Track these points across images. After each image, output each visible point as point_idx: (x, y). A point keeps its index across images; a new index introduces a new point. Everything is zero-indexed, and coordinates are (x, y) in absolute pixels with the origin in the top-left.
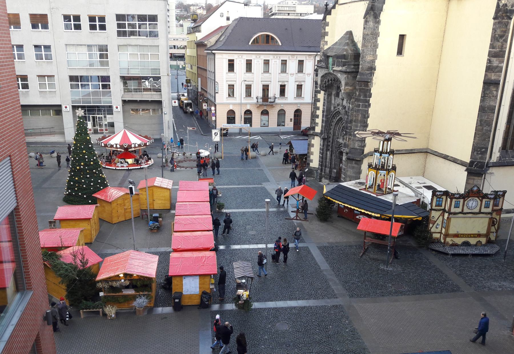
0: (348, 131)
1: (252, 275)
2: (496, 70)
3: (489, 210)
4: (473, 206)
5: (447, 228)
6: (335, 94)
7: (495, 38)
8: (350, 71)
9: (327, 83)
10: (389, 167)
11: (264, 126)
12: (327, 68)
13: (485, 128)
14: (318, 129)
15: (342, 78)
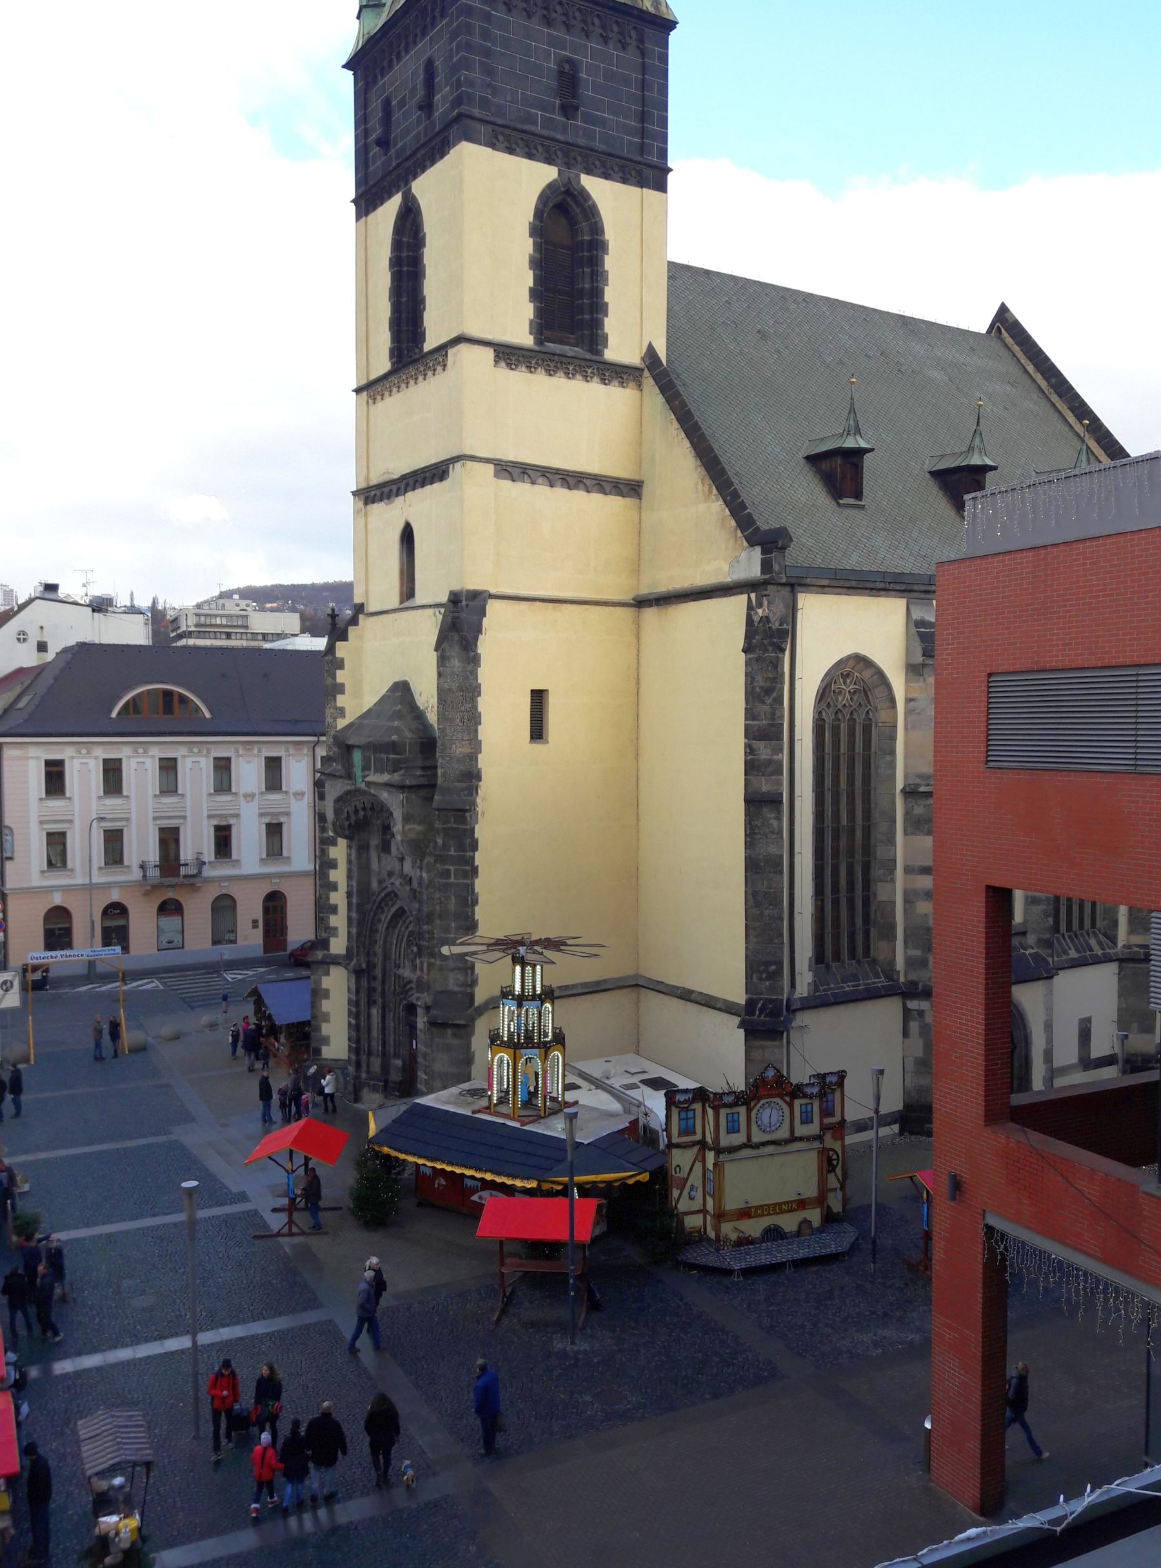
0: (422, 946)
1: (148, 1454)
2: (769, 770)
3: (814, 1129)
4: (773, 1121)
5: (718, 1195)
6: (377, 847)
7: (752, 696)
8: (414, 783)
9: (353, 818)
10: (546, 1036)
11: (170, 946)
12: (350, 776)
13: (767, 912)
14: (338, 946)
15: (395, 803)
